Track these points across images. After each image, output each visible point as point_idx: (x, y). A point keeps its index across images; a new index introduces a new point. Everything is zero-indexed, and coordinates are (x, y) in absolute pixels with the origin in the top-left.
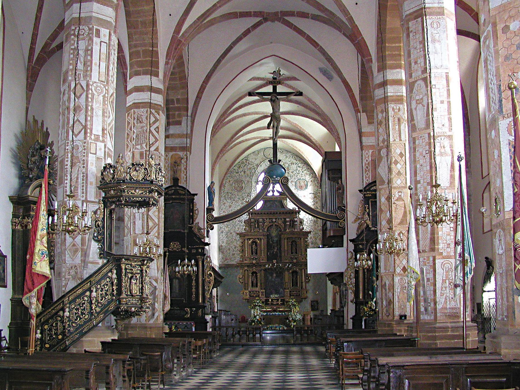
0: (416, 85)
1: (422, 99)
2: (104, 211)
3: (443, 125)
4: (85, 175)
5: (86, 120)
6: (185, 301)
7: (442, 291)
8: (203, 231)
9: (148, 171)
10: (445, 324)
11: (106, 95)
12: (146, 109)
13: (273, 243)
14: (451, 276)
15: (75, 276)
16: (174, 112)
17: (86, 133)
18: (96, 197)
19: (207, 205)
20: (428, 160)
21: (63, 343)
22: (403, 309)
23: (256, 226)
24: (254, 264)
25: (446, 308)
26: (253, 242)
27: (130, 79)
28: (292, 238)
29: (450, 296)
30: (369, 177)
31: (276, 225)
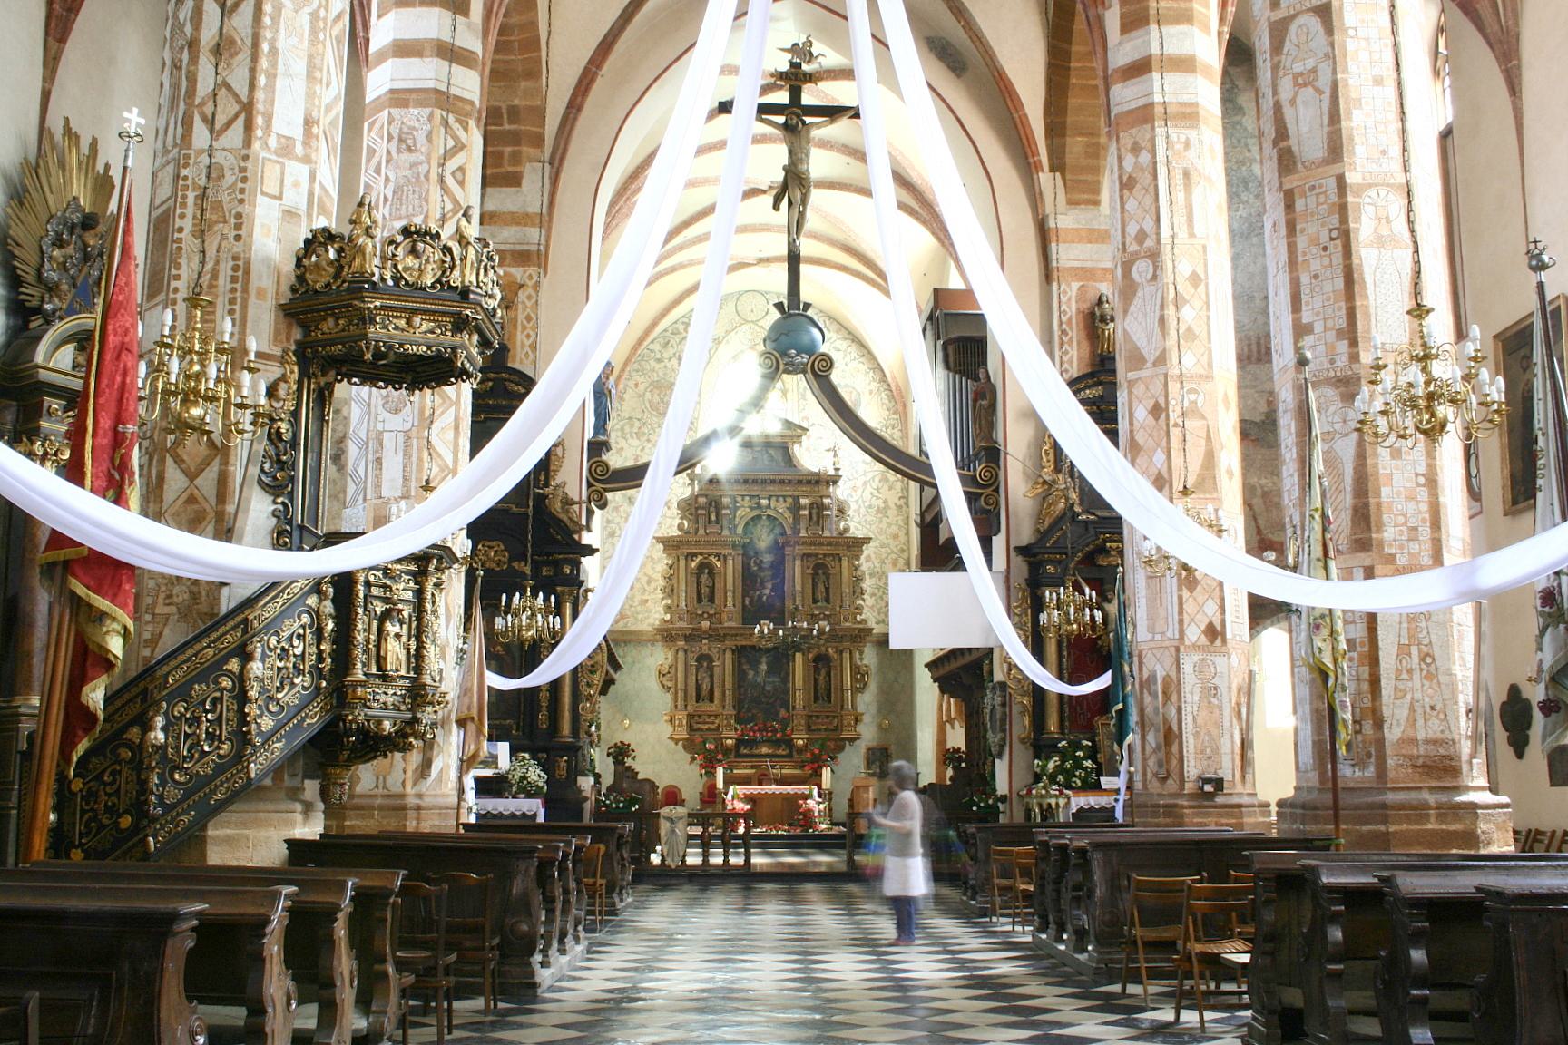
0: (1293, 28)
1: (1314, 70)
2: (300, 390)
3: (1383, 152)
4: (241, 263)
5: (252, 85)
6: (517, 730)
7: (1399, 684)
8: (576, 507)
9: (453, 258)
10: (1413, 796)
11: (322, 13)
12: (428, 110)
13: (760, 568)
14: (1425, 632)
15: (189, 609)
16: (500, 148)
17: (249, 127)
18: (276, 341)
19: (589, 433)
20: (1338, 259)
21: (134, 846)
22: (1209, 758)
23: (713, 517)
24: (705, 632)
25: (1413, 741)
26: (701, 566)
27: (379, 17)
28: (817, 555)
29: (1427, 700)
30: (1071, 362)
31: (769, 516)
